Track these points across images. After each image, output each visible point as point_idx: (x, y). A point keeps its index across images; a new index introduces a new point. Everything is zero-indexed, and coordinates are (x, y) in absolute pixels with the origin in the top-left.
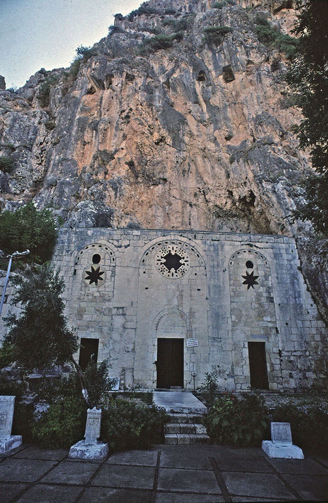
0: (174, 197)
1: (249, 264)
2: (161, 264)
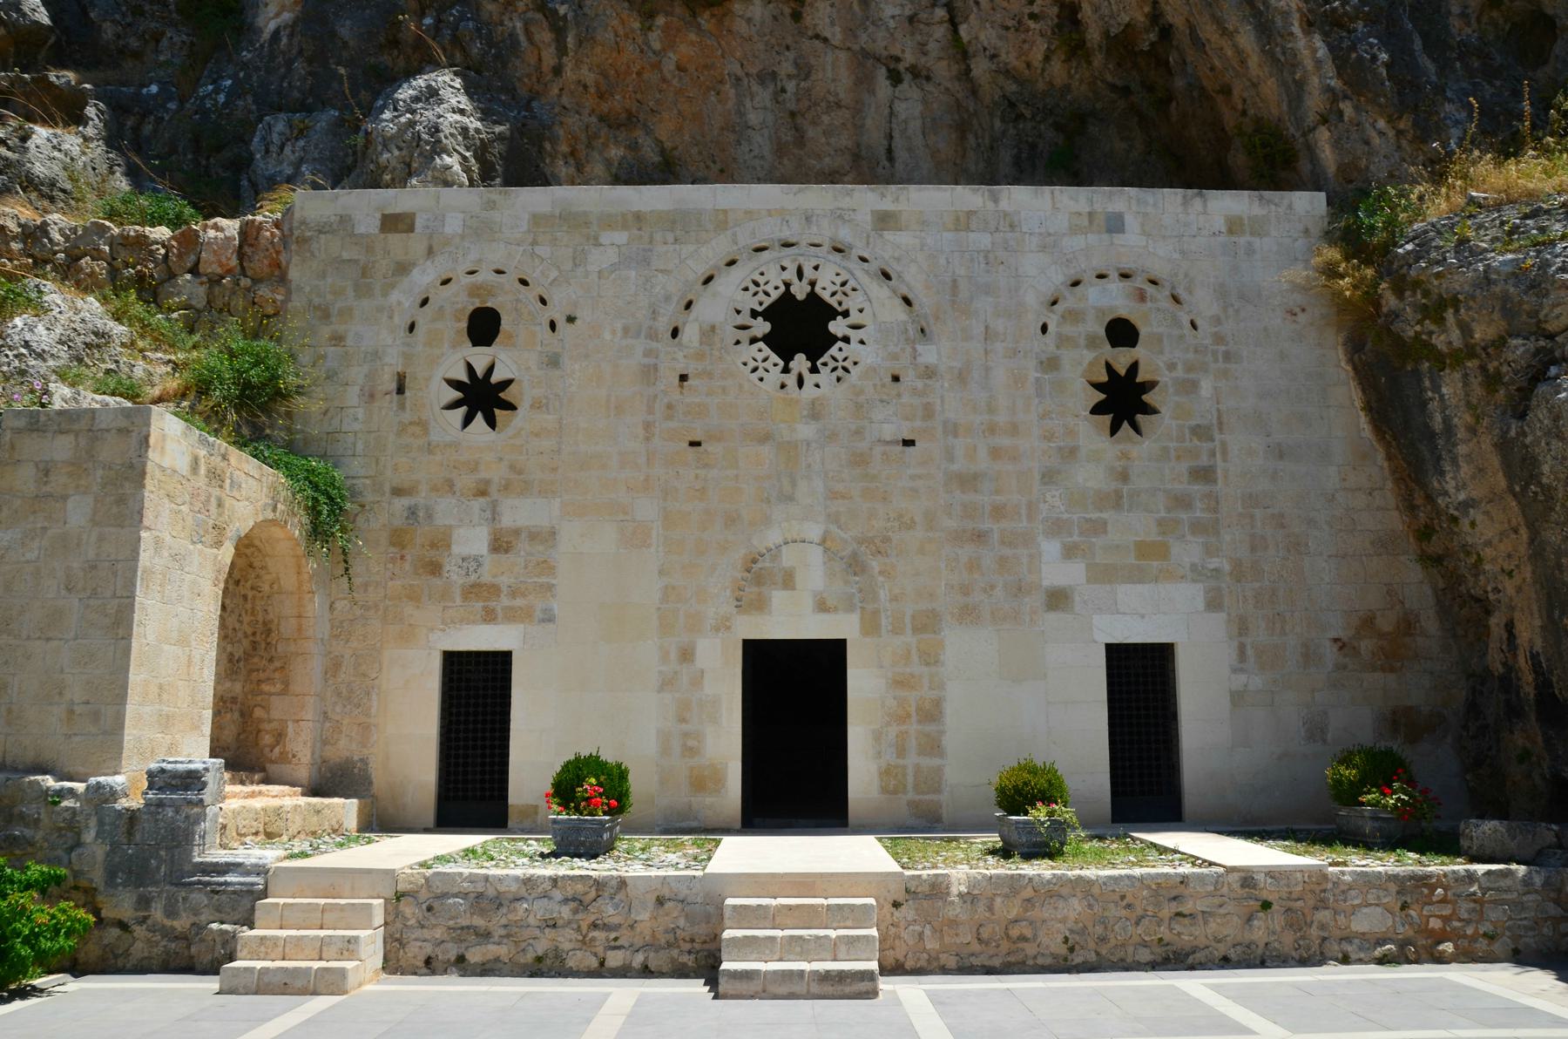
0: (817, 37)
1: (1121, 332)
2: (753, 341)
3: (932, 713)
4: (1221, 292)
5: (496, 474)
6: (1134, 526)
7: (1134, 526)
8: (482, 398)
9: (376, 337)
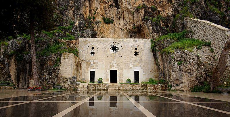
1: (136, 49)
3: (123, 75)
4: (143, 46)
5: (94, 58)
6: (136, 63)
7: (136, 63)
8: (93, 53)
9: (85, 48)
